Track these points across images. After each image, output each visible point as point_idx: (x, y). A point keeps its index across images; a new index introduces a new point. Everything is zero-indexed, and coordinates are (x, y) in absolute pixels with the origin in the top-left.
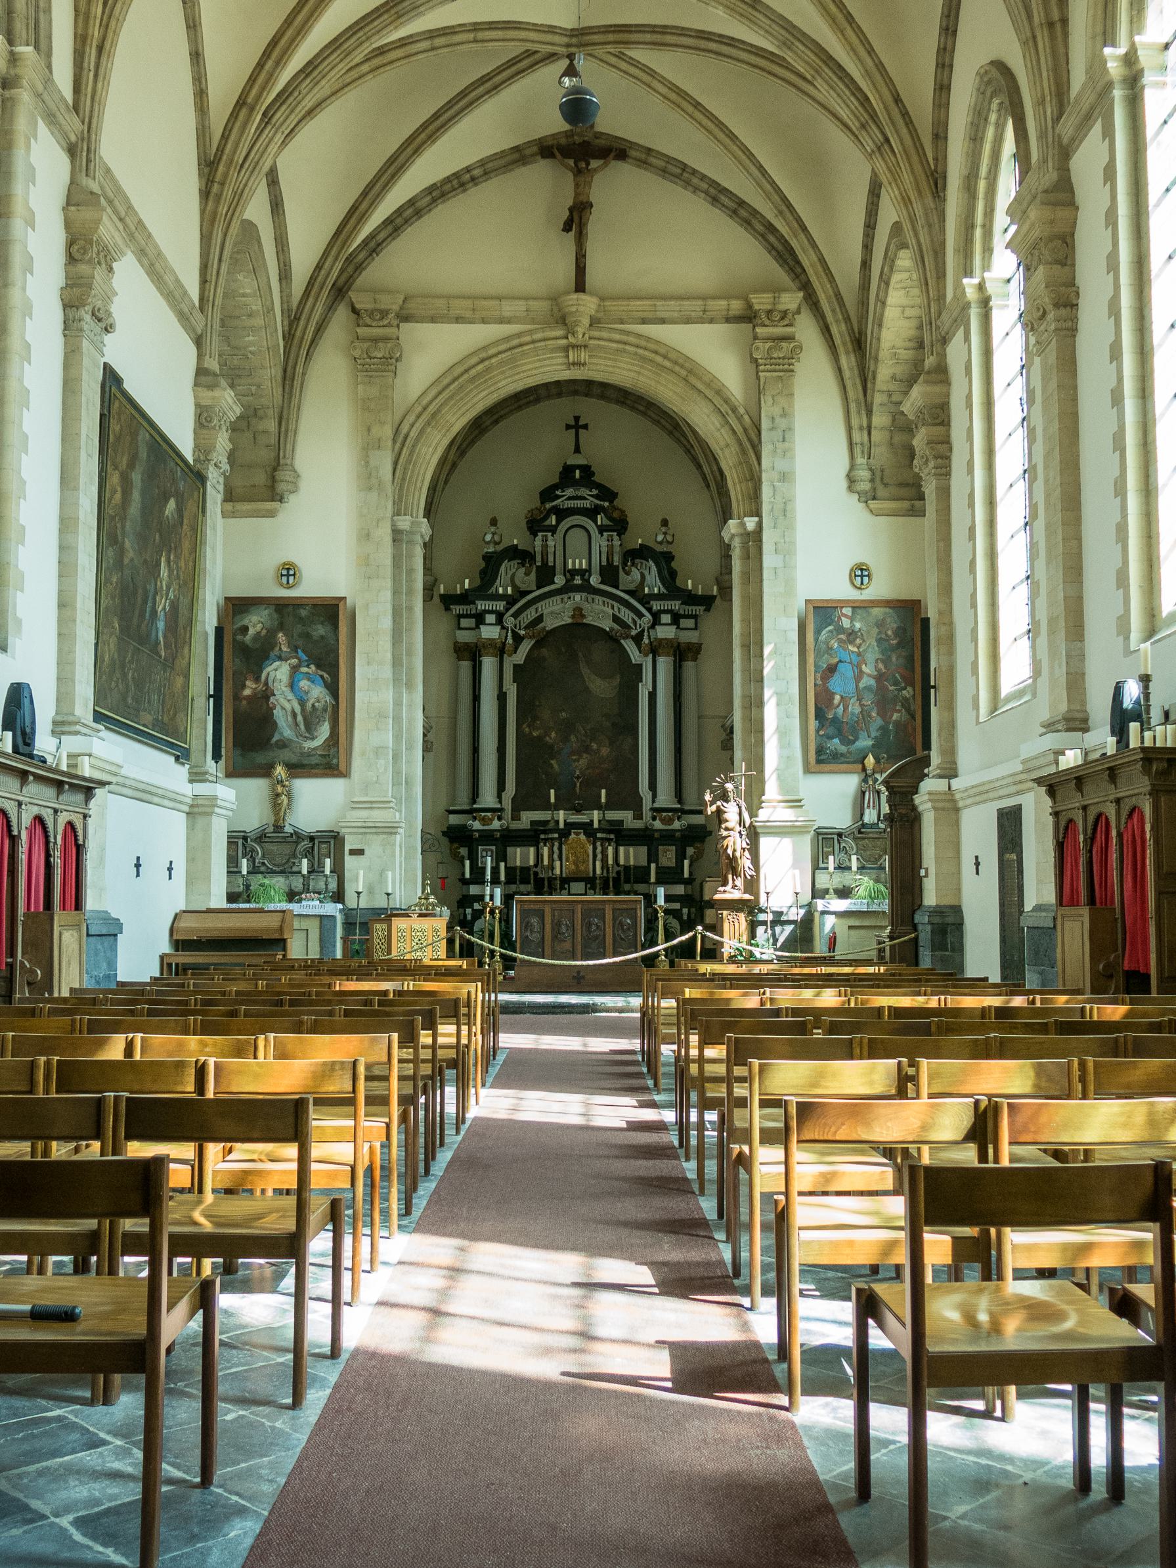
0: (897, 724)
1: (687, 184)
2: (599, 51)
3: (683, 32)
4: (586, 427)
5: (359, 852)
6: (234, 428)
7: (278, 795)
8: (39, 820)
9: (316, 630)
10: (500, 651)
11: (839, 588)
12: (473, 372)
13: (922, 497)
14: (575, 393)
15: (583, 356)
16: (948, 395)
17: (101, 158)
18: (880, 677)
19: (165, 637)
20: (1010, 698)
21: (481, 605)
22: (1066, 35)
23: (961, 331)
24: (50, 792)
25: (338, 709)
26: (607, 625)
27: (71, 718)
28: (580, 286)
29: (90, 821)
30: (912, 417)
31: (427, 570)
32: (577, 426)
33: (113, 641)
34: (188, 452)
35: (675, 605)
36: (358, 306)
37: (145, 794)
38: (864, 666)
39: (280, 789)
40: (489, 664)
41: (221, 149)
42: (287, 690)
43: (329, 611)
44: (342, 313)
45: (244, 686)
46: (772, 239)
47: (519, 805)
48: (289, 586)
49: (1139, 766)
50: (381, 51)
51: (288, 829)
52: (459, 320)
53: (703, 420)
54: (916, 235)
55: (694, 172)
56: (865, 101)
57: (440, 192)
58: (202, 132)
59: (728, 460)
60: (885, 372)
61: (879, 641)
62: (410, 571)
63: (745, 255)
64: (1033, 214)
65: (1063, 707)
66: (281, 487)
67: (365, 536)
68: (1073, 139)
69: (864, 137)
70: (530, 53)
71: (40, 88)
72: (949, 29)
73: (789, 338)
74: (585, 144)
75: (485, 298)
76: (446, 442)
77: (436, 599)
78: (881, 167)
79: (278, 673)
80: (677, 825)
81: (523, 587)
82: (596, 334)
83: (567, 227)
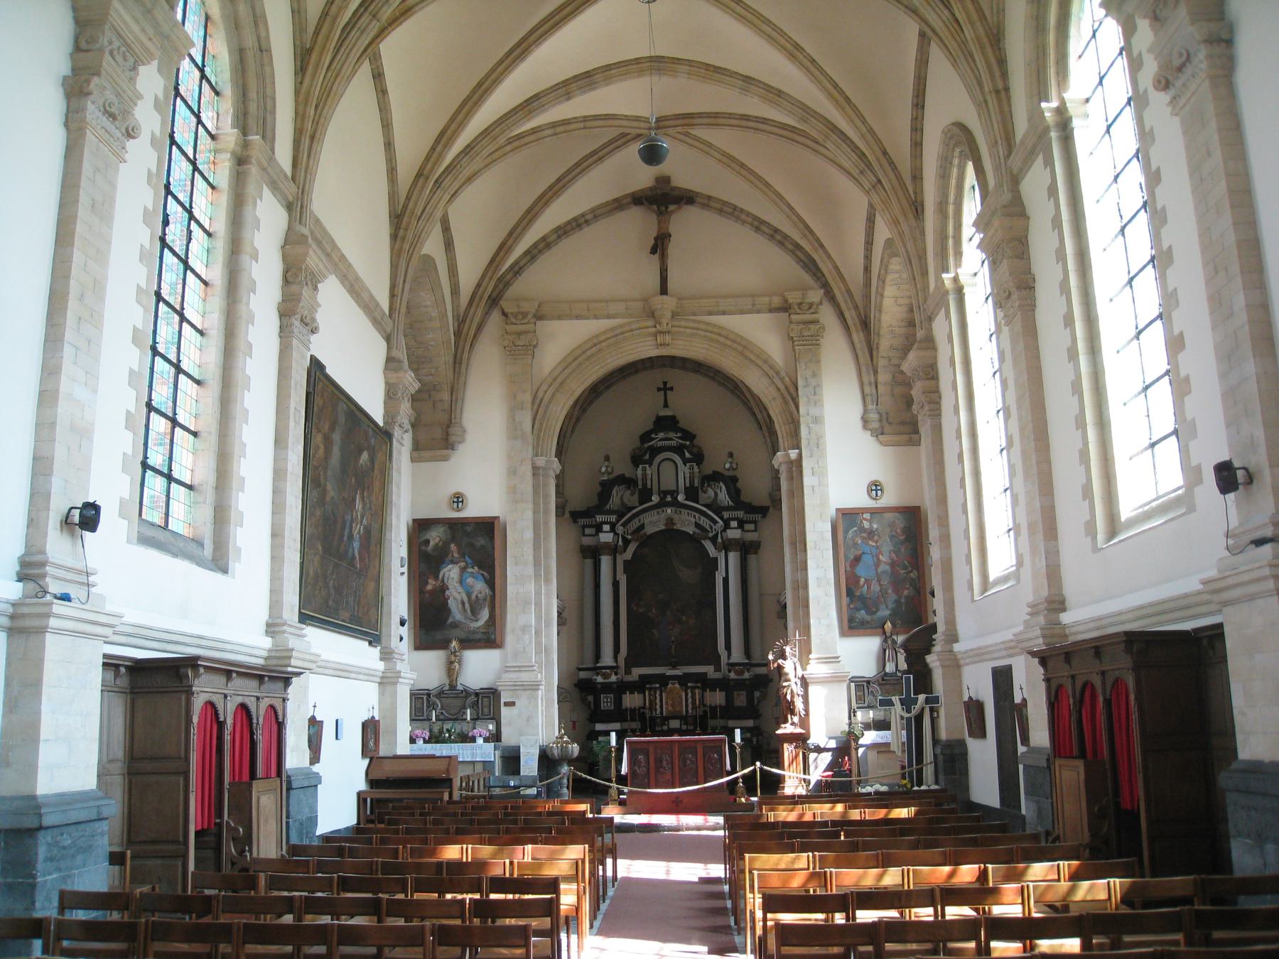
0: (907, 597)
1: (738, 219)
2: (671, 131)
3: (730, 116)
4: (671, 389)
5: (513, 704)
6: (414, 399)
7: (452, 663)
8: (243, 708)
9: (477, 541)
10: (613, 550)
11: (860, 499)
12: (589, 353)
13: (916, 432)
14: (664, 366)
15: (668, 339)
16: (936, 358)
17: (311, 212)
18: (893, 564)
19: (360, 553)
20: (999, 581)
21: (599, 518)
22: (1009, 98)
23: (943, 312)
24: (254, 683)
25: (494, 599)
26: (691, 530)
27: (279, 621)
28: (664, 290)
29: (289, 704)
30: (909, 374)
31: (559, 493)
32: (665, 388)
33: (317, 559)
34: (380, 421)
35: (740, 514)
36: (506, 311)
37: (342, 672)
38: (883, 553)
39: (453, 658)
40: (605, 561)
41: (405, 207)
42: (457, 585)
43: (488, 527)
44: (495, 316)
45: (427, 583)
46: (799, 254)
47: (631, 662)
48: (458, 510)
49: (1122, 646)
50: (519, 137)
51: (460, 687)
52: (578, 317)
53: (756, 382)
54: (905, 246)
55: (742, 211)
56: (862, 156)
57: (564, 231)
58: (393, 196)
59: (775, 411)
60: (886, 344)
61: (891, 537)
62: (546, 496)
63: (784, 267)
64: (996, 223)
65: (1045, 593)
66: (452, 439)
67: (512, 472)
68: (1021, 170)
69: (862, 179)
70: (624, 135)
71: (265, 164)
72: (919, 103)
73: (816, 322)
74: (665, 195)
75: (596, 301)
76: (571, 402)
77: (567, 515)
78: (876, 199)
79: (451, 573)
80: (747, 675)
81: (629, 504)
82: (676, 323)
83: (653, 251)
